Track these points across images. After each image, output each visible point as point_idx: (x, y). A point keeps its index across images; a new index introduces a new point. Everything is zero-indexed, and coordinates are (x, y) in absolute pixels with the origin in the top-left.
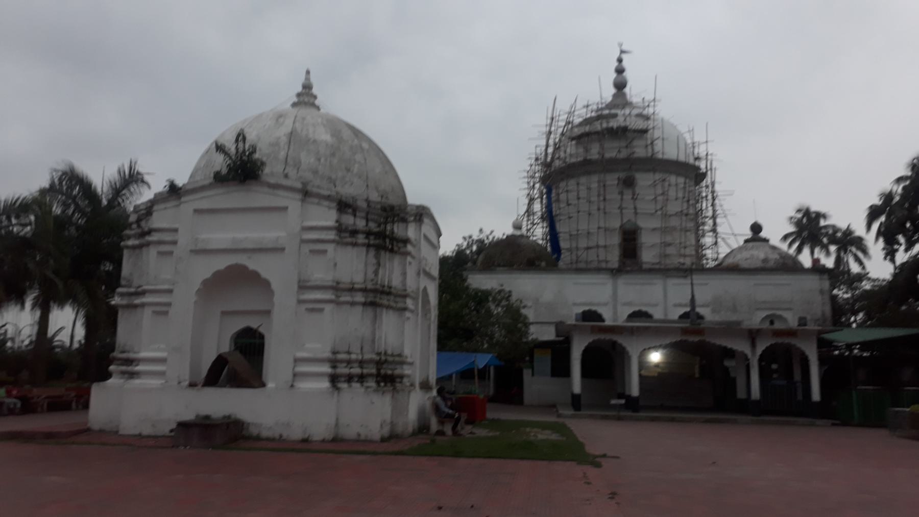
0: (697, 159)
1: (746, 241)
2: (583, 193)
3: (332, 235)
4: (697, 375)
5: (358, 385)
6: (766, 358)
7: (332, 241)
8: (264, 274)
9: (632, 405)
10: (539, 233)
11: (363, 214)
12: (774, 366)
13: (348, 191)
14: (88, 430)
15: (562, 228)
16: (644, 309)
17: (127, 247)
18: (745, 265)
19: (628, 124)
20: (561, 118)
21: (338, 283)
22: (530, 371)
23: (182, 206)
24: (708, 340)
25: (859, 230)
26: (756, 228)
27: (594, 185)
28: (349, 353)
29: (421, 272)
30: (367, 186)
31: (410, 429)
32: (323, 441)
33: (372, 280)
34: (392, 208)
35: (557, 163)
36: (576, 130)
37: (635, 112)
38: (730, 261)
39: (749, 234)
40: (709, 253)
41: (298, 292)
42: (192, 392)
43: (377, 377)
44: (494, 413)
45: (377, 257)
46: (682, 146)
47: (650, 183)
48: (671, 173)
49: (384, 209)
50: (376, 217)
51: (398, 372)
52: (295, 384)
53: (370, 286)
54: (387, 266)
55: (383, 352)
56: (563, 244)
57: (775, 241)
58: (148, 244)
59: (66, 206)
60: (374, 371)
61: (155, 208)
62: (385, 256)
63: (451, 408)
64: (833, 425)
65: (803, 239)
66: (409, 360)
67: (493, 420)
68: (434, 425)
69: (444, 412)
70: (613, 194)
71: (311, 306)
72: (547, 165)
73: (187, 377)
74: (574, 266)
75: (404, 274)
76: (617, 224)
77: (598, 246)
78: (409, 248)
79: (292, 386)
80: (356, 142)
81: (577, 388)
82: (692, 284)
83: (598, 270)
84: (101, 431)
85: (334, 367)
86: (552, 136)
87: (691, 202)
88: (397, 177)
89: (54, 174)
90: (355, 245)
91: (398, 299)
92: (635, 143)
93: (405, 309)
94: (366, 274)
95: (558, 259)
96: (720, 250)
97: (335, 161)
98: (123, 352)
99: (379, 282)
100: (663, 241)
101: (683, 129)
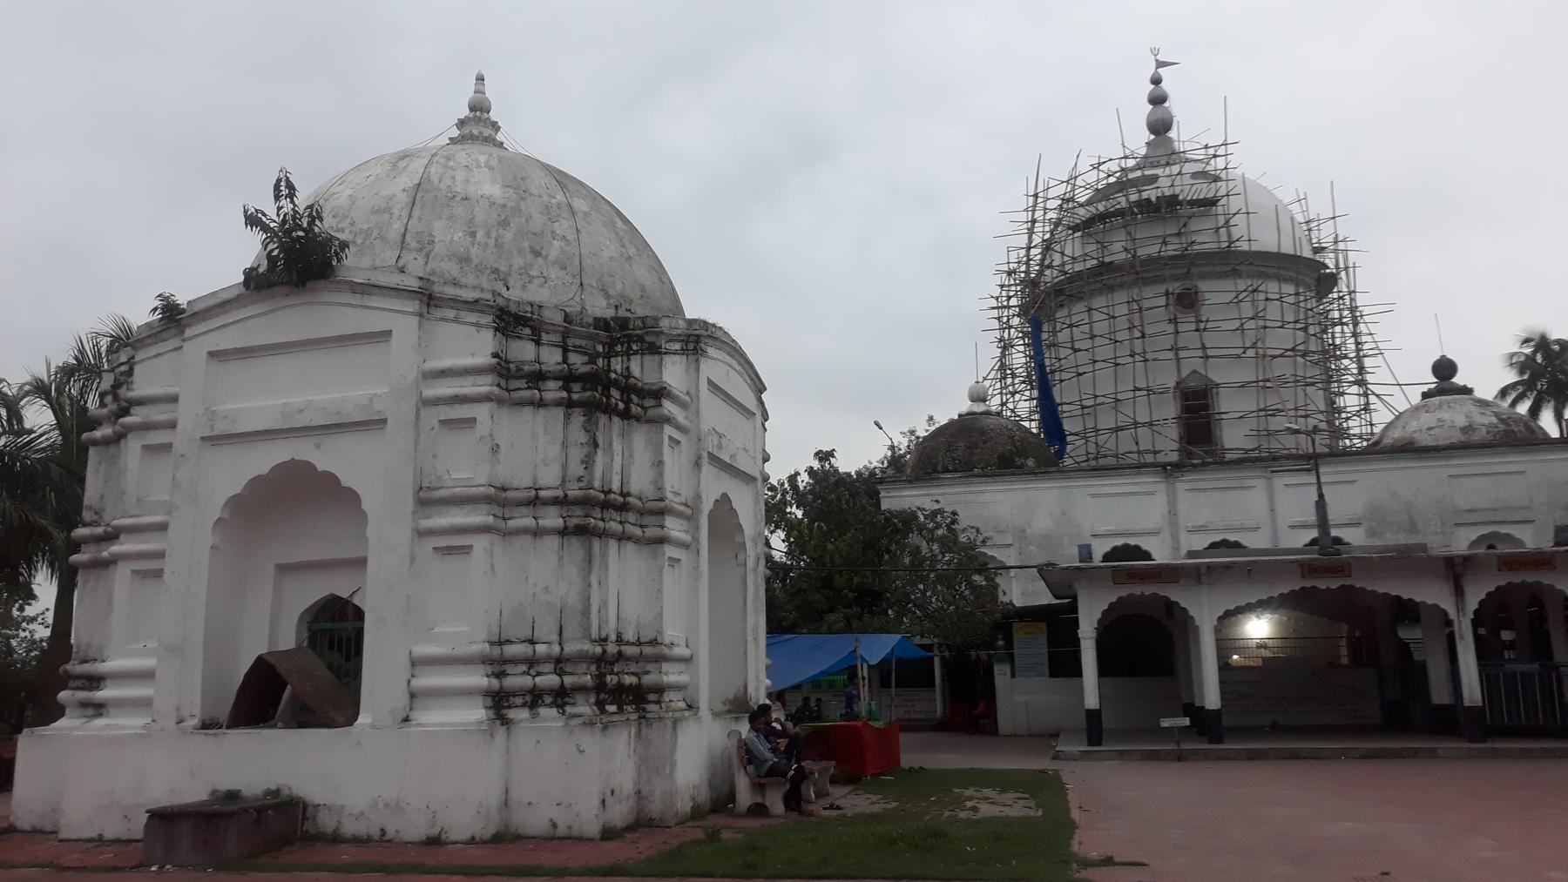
0: (1319, 250)
1: (1425, 395)
2: (1101, 327)
3: (484, 385)
4: (1345, 661)
5: (554, 712)
6: (1490, 616)
7: (487, 398)
8: (346, 480)
9: (1205, 725)
10: (1024, 406)
11: (557, 338)
12: (1506, 635)
13: (518, 295)
14: (12, 829)
17: (95, 443)
18: (1426, 440)
19: (1177, 190)
20: (1051, 193)
21: (504, 489)
22: (1007, 668)
23: (187, 346)
24: (1559, 586)
26: (1445, 369)
27: (1123, 309)
28: (532, 642)
29: (705, 461)
30: (581, 284)
31: (684, 805)
33: (579, 480)
34: (623, 323)
36: (1081, 211)
37: (1189, 168)
38: (1396, 434)
40: (1355, 427)
41: (414, 513)
42: (205, 741)
43: (598, 694)
44: (915, 754)
46: (1286, 225)
47: (1229, 297)
48: (1268, 277)
50: (584, 343)
51: (648, 680)
52: (413, 715)
53: (574, 493)
54: (617, 446)
55: (613, 637)
56: (1068, 426)
57: (1486, 390)
60: (587, 679)
65: (1540, 392)
66: (680, 651)
67: (911, 770)
68: (745, 796)
71: (443, 542)
72: (1030, 284)
73: (197, 710)
74: (1093, 463)
75: (659, 464)
77: (1136, 424)
78: (668, 407)
79: (406, 720)
80: (560, 197)
81: (1091, 700)
82: (1319, 484)
83: (1139, 467)
84: (35, 831)
85: (500, 675)
86: (1038, 227)
87: (1312, 330)
88: (658, 269)
90: (540, 404)
91: (647, 520)
92: (1194, 225)
93: (662, 541)
94: (565, 466)
95: (1060, 454)
96: (1376, 417)
97: (508, 236)
99: (597, 484)
100: (1262, 406)
101: (1285, 196)
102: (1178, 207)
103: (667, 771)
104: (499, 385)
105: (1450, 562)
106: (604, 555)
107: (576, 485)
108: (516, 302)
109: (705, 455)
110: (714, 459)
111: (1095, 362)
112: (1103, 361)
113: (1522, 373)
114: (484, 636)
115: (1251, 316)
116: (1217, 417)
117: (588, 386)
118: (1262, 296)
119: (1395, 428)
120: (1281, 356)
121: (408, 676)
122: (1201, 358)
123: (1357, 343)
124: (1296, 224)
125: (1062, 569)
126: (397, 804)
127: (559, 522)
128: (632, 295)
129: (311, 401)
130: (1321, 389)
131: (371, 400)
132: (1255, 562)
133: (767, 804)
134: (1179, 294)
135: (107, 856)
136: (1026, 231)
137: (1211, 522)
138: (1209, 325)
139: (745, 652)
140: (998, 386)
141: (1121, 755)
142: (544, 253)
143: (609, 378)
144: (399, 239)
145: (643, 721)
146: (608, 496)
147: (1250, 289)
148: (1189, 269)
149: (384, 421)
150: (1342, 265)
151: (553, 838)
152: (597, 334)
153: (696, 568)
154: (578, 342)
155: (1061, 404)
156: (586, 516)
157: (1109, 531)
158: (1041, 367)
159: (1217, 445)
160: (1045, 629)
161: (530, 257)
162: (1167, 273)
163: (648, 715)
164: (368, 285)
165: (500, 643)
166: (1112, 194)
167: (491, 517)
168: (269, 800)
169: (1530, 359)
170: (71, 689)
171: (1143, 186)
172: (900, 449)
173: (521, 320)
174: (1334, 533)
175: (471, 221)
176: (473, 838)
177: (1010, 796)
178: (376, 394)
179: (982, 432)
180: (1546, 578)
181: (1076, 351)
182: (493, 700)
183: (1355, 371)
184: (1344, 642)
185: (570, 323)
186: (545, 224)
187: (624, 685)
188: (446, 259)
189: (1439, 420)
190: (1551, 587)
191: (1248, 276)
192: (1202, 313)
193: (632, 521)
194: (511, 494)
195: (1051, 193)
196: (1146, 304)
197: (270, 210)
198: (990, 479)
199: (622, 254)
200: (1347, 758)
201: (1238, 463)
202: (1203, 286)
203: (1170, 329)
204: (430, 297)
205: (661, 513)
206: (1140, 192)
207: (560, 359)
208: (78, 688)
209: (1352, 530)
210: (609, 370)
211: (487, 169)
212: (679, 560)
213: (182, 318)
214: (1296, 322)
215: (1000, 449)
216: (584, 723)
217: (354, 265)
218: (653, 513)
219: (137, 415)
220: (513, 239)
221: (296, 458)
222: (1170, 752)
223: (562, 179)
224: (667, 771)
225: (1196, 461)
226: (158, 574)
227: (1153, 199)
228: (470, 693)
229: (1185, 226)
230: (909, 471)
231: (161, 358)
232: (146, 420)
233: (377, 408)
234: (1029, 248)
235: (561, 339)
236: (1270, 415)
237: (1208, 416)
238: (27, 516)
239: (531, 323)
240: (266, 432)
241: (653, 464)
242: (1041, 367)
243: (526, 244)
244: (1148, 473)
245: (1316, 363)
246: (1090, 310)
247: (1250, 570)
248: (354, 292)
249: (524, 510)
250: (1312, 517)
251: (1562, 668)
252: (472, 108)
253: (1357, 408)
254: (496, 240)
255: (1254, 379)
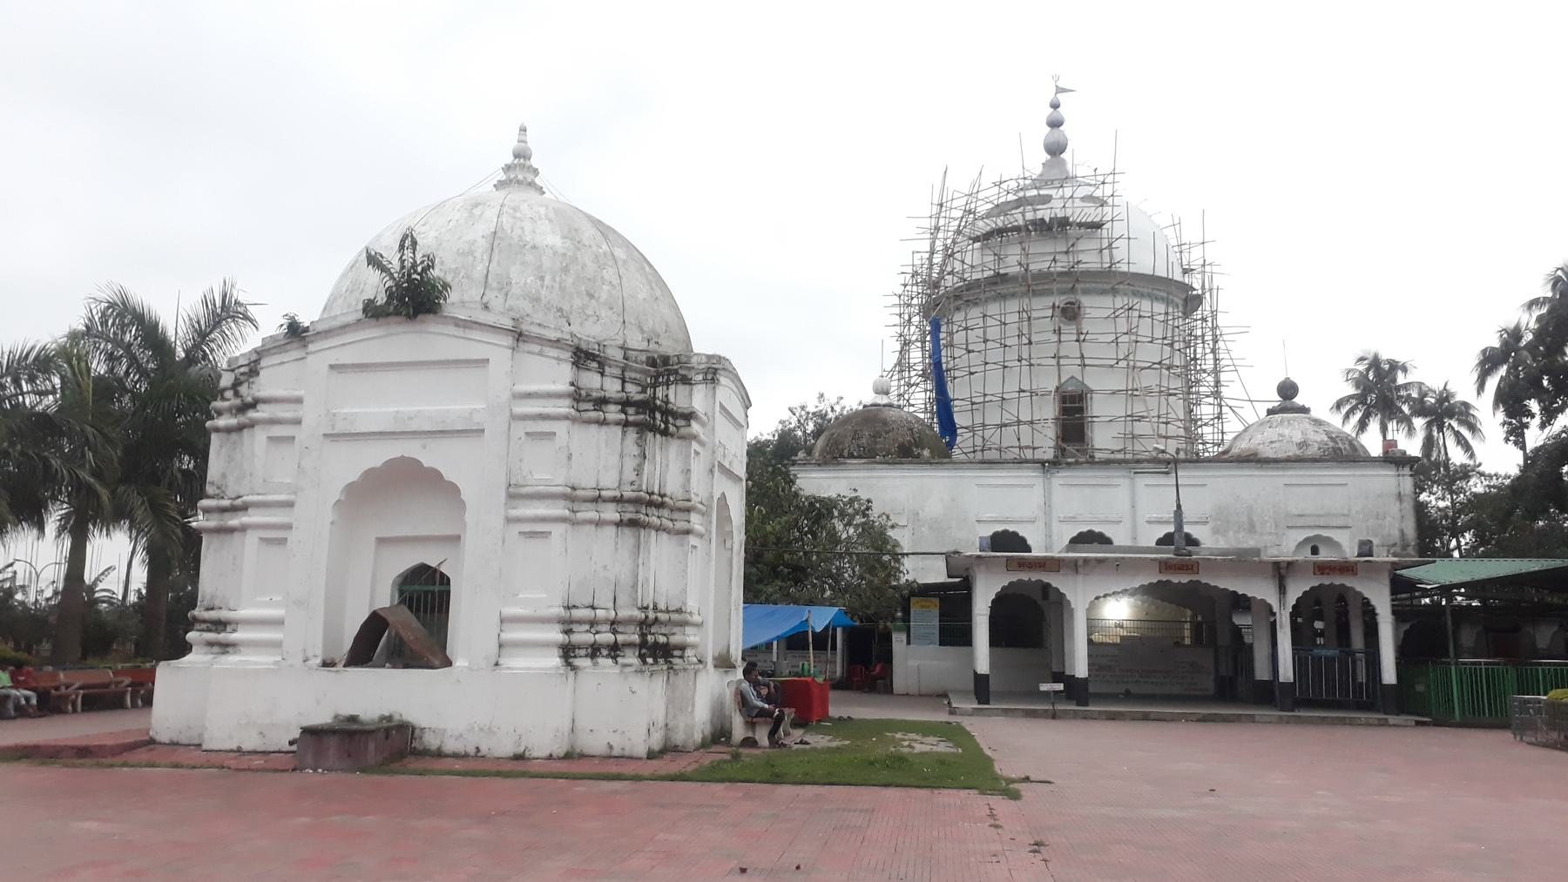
1: (1270, 412)
2: (993, 333)
3: (564, 407)
4: (1187, 641)
5: (610, 661)
7: (566, 417)
8: (449, 475)
9: (1076, 691)
10: (919, 400)
11: (617, 372)
13: (590, 332)
15: (956, 391)
16: (1097, 529)
17: (217, 430)
18: (1268, 452)
19: (1069, 212)
20: (956, 203)
21: (574, 488)
22: (904, 637)
23: (310, 358)
24: (1358, 589)
25: (1464, 390)
26: (1288, 390)
28: (593, 608)
31: (698, 737)
32: (550, 757)
34: (666, 360)
35: (949, 281)
37: (1082, 192)
38: (1243, 446)
39: (1275, 399)
40: (1208, 432)
41: (506, 504)
42: (325, 672)
45: (641, 443)
48: (1142, 296)
49: (652, 362)
50: (638, 376)
51: (674, 640)
52: (501, 662)
53: (628, 494)
55: (651, 606)
56: (959, 419)
58: (252, 425)
59: (111, 358)
60: (636, 638)
61: (263, 363)
62: (654, 441)
63: (767, 700)
64: (1418, 723)
65: (1369, 406)
66: (696, 618)
67: (840, 719)
68: (739, 731)
69: (757, 707)
70: (1044, 330)
71: (527, 528)
73: (319, 652)
74: (979, 456)
75: (687, 471)
76: (1051, 385)
77: (1019, 422)
78: (695, 427)
79: (497, 664)
80: (605, 247)
81: (983, 666)
83: (1020, 462)
85: (568, 632)
86: (940, 235)
87: (1176, 346)
88: (674, 306)
89: (92, 306)
90: (603, 423)
91: (676, 515)
92: (1081, 246)
93: (688, 532)
94: (621, 472)
95: (951, 445)
98: (208, 609)
99: (644, 487)
100: (1129, 413)
101: (1163, 220)
102: (1068, 228)
103: (690, 709)
104: (573, 407)
105: (1277, 565)
106: (647, 542)
107: (629, 488)
108: (586, 341)
109: (716, 464)
110: (721, 466)
111: (986, 363)
112: (994, 363)
113: (1357, 387)
114: (560, 602)
115: (1125, 331)
116: (1090, 419)
117: (641, 410)
118: (1136, 314)
119: (1244, 439)
120: (1149, 368)
121: (499, 631)
122: (1079, 365)
123: (1216, 360)
124: (1170, 247)
125: (967, 556)
126: (489, 729)
127: (617, 517)
128: (659, 330)
129: (419, 411)
130: (1180, 399)
131: (471, 414)
132: (1123, 558)
133: (757, 738)
134: (1063, 308)
135: (258, 762)
136: (928, 236)
137: (1081, 514)
138: (1088, 337)
139: (729, 620)
140: (896, 377)
141: (1006, 712)
142: (596, 295)
143: (654, 404)
144: (483, 280)
145: (671, 671)
146: (652, 497)
147: (1126, 307)
148: (1074, 286)
149: (483, 431)
150: (1207, 286)
151: (610, 757)
152: (649, 370)
153: (708, 554)
154: (633, 375)
155: (954, 400)
156: (637, 512)
157: (992, 517)
158: (937, 364)
159: (1088, 445)
160: (938, 604)
161: (587, 299)
162: (1055, 286)
163: (675, 667)
164: (471, 321)
165: (568, 608)
166: (1010, 210)
167: (567, 511)
168: (385, 724)
169: (1364, 376)
170: (198, 630)
171: (1038, 205)
172: (790, 423)
173: (590, 356)
174: (1187, 529)
175: (540, 266)
176: (551, 755)
177: (931, 739)
178: (475, 409)
179: (885, 423)
180: (1349, 582)
181: (969, 352)
182: (563, 651)
183: (1212, 384)
184: (1187, 626)
185: (627, 360)
186: (596, 271)
187: (658, 643)
188: (521, 298)
189: (1279, 435)
190: (1352, 589)
191: (1125, 294)
192: (1083, 326)
193: (666, 516)
194: (579, 493)
195: (956, 203)
196: (1034, 314)
197: (392, 259)
198: (891, 467)
199: (652, 296)
200: (1187, 721)
201: (1107, 463)
202: (1086, 301)
203: (1055, 338)
204: (520, 334)
205: (688, 510)
206: (1035, 210)
207: (620, 388)
208: (203, 630)
209: (1199, 527)
210: (654, 398)
211: (547, 221)
212: (696, 547)
213: (306, 336)
214: (1164, 338)
215: (901, 439)
216: (636, 671)
217: (454, 303)
218: (680, 510)
219: (263, 412)
220: (573, 283)
221: (405, 455)
222: (1046, 711)
223: (604, 231)
224: (690, 709)
225: (1070, 460)
226: (282, 542)
227: (1047, 220)
228: (548, 646)
229: (1073, 245)
230: (817, 454)
231: (281, 367)
232: (271, 416)
233: (476, 421)
234: (932, 252)
235: (621, 372)
236: (1136, 420)
237: (1082, 418)
238: (75, 473)
239: (598, 359)
240: (381, 433)
241: (682, 471)
242: (937, 364)
243: (583, 288)
244: (1028, 468)
245: (1179, 376)
246: (985, 316)
247: (1118, 565)
248: (457, 325)
249: (588, 504)
250: (1169, 515)
251: (1358, 654)
252: (516, 156)
253: (1212, 417)
254: (560, 284)
255: (1125, 389)
